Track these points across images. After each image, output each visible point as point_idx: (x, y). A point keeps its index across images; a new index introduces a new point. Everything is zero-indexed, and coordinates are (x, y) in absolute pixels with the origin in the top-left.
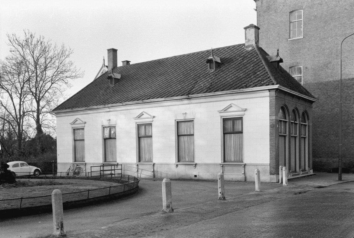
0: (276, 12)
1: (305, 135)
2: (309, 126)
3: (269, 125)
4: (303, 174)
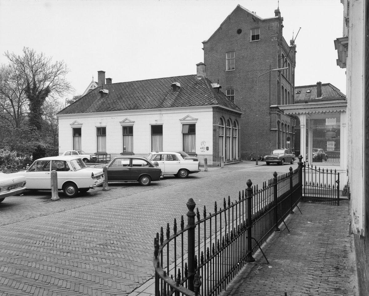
0: (217, 52)
1: (236, 136)
2: (238, 130)
3: (212, 130)
4: (234, 161)
